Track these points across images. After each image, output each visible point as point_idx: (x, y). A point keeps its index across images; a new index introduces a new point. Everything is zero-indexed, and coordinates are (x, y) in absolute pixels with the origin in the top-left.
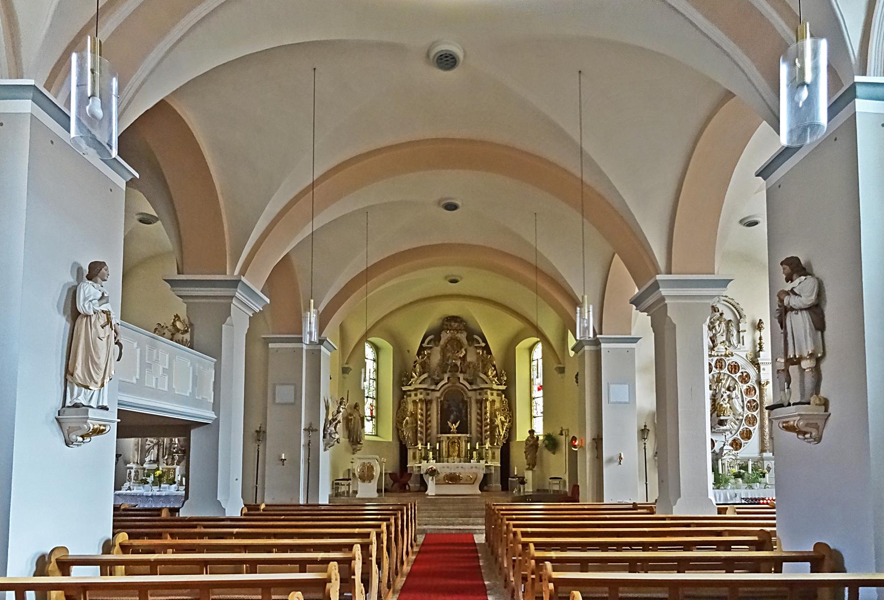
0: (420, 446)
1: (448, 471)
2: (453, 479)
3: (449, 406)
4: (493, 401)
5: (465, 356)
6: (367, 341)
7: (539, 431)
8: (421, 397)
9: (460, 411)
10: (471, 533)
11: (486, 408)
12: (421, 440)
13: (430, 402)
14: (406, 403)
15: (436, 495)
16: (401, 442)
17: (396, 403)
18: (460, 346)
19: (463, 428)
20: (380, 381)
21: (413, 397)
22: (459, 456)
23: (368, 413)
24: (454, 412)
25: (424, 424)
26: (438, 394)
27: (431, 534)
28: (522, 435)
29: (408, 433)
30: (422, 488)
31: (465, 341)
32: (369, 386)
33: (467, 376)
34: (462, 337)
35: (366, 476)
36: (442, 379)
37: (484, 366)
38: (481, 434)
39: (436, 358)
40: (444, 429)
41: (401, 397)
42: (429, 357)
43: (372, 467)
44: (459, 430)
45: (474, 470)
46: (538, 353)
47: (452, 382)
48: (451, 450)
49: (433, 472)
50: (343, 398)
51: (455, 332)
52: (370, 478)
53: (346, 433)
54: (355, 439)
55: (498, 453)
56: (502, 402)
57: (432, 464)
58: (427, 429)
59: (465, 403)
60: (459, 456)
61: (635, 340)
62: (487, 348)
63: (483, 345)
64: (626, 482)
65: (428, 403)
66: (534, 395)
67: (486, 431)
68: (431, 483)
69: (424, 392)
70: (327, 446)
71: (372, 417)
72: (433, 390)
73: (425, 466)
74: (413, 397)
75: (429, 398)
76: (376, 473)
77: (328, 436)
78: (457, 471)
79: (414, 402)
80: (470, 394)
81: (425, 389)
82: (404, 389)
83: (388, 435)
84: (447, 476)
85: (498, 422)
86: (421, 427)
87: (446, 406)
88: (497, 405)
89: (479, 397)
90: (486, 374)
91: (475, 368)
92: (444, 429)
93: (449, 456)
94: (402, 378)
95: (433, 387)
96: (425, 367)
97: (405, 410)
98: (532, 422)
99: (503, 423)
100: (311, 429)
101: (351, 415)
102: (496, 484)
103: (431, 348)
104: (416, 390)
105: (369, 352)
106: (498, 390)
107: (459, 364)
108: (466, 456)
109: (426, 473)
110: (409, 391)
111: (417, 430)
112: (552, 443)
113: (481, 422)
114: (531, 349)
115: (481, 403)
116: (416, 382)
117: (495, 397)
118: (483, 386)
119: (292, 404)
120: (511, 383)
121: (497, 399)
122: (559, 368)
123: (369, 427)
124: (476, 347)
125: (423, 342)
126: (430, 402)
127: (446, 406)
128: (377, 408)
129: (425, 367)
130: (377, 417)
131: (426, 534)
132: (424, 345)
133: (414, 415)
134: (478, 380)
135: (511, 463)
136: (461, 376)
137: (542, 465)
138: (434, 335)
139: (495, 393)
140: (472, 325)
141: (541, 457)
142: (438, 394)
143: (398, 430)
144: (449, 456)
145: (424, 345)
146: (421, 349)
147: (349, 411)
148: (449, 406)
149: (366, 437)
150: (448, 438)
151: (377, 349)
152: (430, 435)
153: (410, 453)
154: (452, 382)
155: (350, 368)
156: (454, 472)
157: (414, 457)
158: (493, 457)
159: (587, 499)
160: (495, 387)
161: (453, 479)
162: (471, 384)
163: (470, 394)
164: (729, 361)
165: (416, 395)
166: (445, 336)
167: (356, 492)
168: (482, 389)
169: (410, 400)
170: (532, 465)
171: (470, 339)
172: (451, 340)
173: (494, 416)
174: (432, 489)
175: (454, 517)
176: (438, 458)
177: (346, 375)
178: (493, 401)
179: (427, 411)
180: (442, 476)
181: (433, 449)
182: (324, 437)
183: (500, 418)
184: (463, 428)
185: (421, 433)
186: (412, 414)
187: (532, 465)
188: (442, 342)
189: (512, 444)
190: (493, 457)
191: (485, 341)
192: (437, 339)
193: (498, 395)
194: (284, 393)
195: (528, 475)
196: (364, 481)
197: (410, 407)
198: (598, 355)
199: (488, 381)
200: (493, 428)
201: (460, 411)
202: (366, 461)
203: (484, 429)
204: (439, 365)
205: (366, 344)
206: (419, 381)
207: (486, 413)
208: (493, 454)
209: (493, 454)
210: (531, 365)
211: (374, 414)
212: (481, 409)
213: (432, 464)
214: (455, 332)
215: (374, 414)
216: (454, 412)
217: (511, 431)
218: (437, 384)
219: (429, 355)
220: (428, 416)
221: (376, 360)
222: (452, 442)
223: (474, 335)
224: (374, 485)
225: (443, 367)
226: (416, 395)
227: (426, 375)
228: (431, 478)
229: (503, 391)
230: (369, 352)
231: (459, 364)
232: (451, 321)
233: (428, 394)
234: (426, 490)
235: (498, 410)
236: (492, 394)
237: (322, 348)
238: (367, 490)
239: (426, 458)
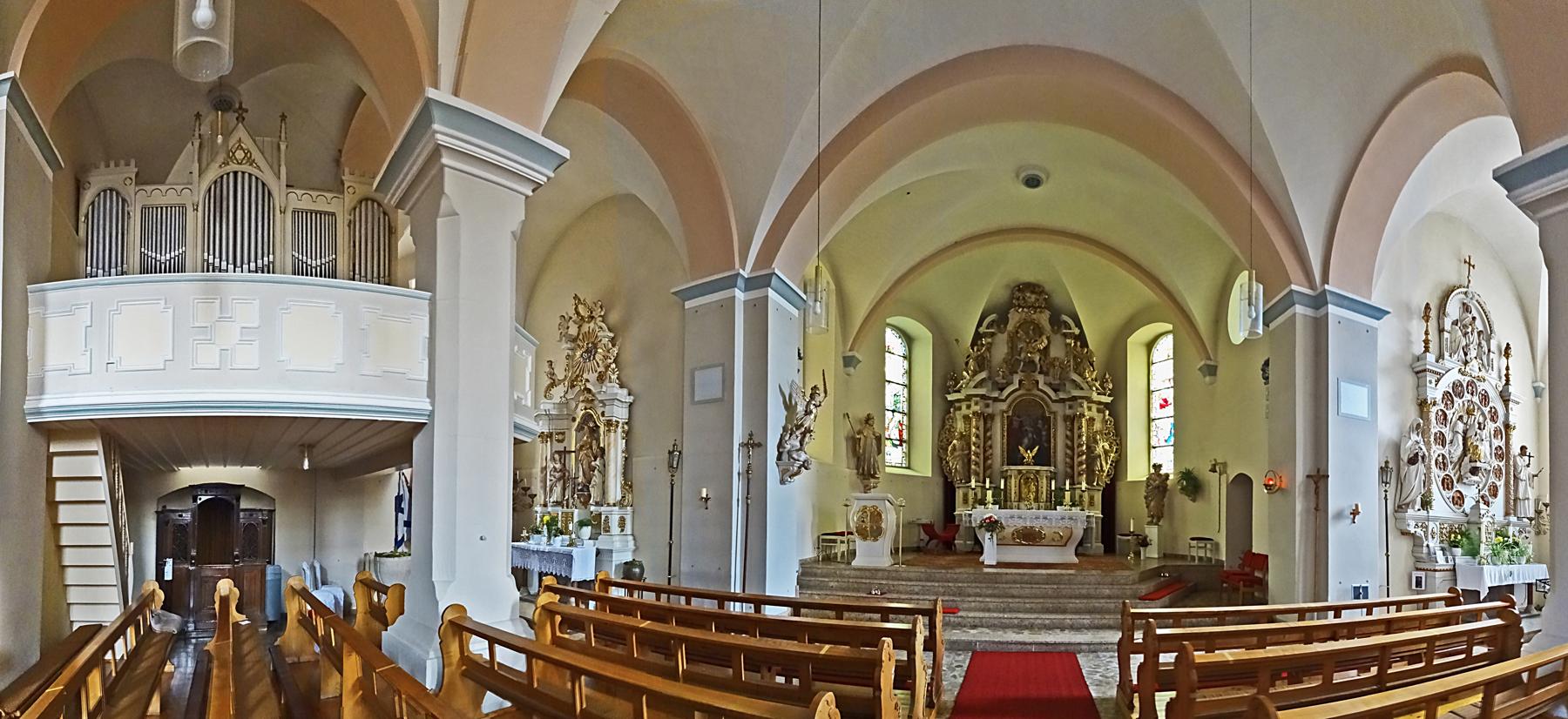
0: (973, 484)
1: (1020, 524)
2: (1029, 537)
3: (1021, 424)
4: (1091, 420)
5: (1046, 348)
6: (889, 325)
7: (1168, 468)
8: (976, 408)
9: (1038, 431)
10: (1066, 657)
11: (1080, 428)
12: (977, 474)
13: (991, 417)
14: (954, 419)
15: (1000, 565)
16: (946, 478)
17: (938, 423)
18: (1039, 331)
19: (1044, 458)
20: (915, 388)
21: (964, 411)
22: (1036, 499)
23: (895, 434)
24: (1030, 432)
25: (980, 451)
26: (1004, 406)
27: (984, 653)
28: (1137, 471)
29: (955, 465)
30: (977, 549)
31: (1047, 326)
32: (893, 394)
33: (1050, 379)
34: (1044, 318)
35: (871, 528)
36: (1009, 383)
37: (1077, 365)
38: (1072, 467)
39: (1000, 350)
40: (1013, 458)
41: (945, 411)
42: (988, 349)
43: (879, 515)
44: (1038, 460)
45: (1067, 523)
46: (1165, 347)
47: (1026, 384)
48: (1024, 490)
49: (992, 525)
50: (815, 388)
51: (1031, 310)
52: (876, 533)
53: (853, 462)
54: (866, 467)
55: (1098, 497)
56: (1105, 422)
57: (992, 511)
58: (986, 459)
59: (1047, 421)
60: (1036, 499)
61: (1378, 313)
62: (1081, 338)
63: (1077, 331)
64: (1363, 562)
65: (987, 419)
66: (1153, 416)
67: (1081, 463)
68: (988, 541)
69: (981, 404)
70: (786, 475)
71: (901, 441)
72: (996, 400)
73: (980, 513)
74: (964, 411)
75: (990, 410)
76: (890, 520)
77: (785, 457)
78: (1037, 525)
79: (966, 418)
80: (1055, 407)
81: (983, 397)
82: (950, 398)
83: (925, 467)
84: (1017, 531)
85: (1099, 450)
86: (977, 454)
87: (1016, 424)
88: (1097, 426)
89: (1069, 412)
90: (1081, 375)
91: (1063, 368)
92: (1013, 458)
93: (1020, 499)
94: (946, 381)
95: (995, 394)
96: (982, 363)
97: (951, 431)
98: (1152, 449)
99: (1106, 452)
100: (754, 444)
101: (860, 432)
102: (1097, 546)
103: (992, 335)
104: (968, 398)
105: (893, 340)
106: (1100, 403)
107: (1037, 359)
108: (1049, 499)
109: (981, 526)
110: (959, 401)
111: (969, 460)
112: (1192, 485)
113: (1072, 449)
114: (1150, 346)
115: (1072, 420)
116: (969, 386)
117: (1094, 413)
118: (1076, 393)
119: (720, 400)
120: (1119, 391)
121: (1098, 417)
122: (1208, 366)
123: (894, 455)
124: (1065, 335)
125: (980, 324)
126: (991, 417)
127: (1016, 424)
128: (909, 427)
129: (982, 363)
130: (909, 442)
131: (975, 653)
132: (982, 330)
133: (965, 438)
134: (1068, 386)
135: (1118, 516)
136: (1041, 378)
137: (1171, 520)
138: (997, 316)
139: (1094, 407)
140: (1058, 300)
141: (1171, 504)
142: (1004, 406)
143: (941, 459)
144: (1020, 499)
145: (982, 330)
146: (978, 336)
147: (858, 428)
148: (1021, 424)
149: (888, 470)
150: (1020, 472)
151: (908, 339)
152: (990, 467)
153: (959, 494)
154: (1026, 384)
155: (860, 356)
156: (1029, 525)
157: (966, 501)
158: (1091, 503)
159: (1286, 590)
160: (1095, 397)
161: (1029, 537)
162: (1056, 391)
163: (1055, 407)
164: (1481, 386)
165: (969, 407)
166: (1014, 318)
167: (853, 554)
168: (1074, 398)
169: (959, 415)
170: (1156, 518)
171: (1056, 322)
172: (1024, 324)
173: (1092, 441)
174: (990, 555)
175: (1031, 611)
176: (1002, 500)
177: (851, 370)
178: (1091, 420)
179: (986, 431)
180: (1009, 531)
181: (996, 489)
182: (779, 458)
183: (1103, 445)
184: (1044, 458)
185: (977, 464)
186: (962, 437)
187: (1156, 518)
188: (1010, 327)
189: (1120, 486)
190: (1091, 503)
191: (1079, 325)
192: (1002, 321)
193: (1099, 411)
194: (707, 384)
195: (1152, 532)
196: (865, 538)
197: (960, 426)
198: (1319, 328)
199: (1085, 386)
200: (1092, 459)
201: (1039, 435)
202: (869, 504)
203: (1076, 461)
204: (1005, 361)
205: (888, 330)
206: (972, 384)
207: (1080, 436)
208: (1092, 498)
209: (1092, 498)
210: (1154, 371)
211: (905, 436)
212: (1072, 430)
213: (992, 511)
214: (1031, 310)
215: (905, 436)
216: (1030, 432)
217: (1119, 465)
218: (1002, 390)
219: (990, 347)
220: (987, 438)
221: (908, 357)
222: (1025, 479)
223: (1062, 319)
224: (886, 543)
225: (1011, 365)
226: (969, 407)
227: (983, 375)
228: (988, 535)
229: (1107, 405)
230: (893, 340)
231: (1037, 359)
232: (1027, 294)
233: (987, 406)
234: (981, 553)
235: (1101, 432)
236: (1090, 409)
237: (771, 292)
238: (873, 555)
239: (983, 502)
